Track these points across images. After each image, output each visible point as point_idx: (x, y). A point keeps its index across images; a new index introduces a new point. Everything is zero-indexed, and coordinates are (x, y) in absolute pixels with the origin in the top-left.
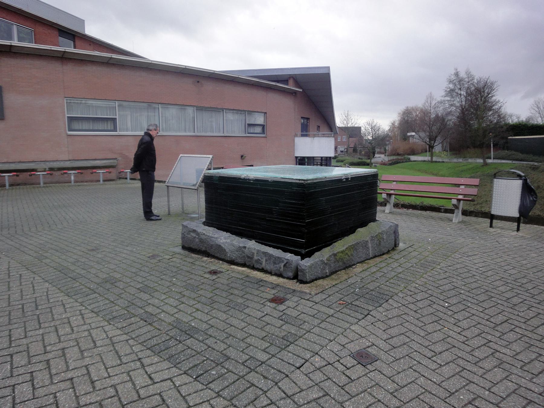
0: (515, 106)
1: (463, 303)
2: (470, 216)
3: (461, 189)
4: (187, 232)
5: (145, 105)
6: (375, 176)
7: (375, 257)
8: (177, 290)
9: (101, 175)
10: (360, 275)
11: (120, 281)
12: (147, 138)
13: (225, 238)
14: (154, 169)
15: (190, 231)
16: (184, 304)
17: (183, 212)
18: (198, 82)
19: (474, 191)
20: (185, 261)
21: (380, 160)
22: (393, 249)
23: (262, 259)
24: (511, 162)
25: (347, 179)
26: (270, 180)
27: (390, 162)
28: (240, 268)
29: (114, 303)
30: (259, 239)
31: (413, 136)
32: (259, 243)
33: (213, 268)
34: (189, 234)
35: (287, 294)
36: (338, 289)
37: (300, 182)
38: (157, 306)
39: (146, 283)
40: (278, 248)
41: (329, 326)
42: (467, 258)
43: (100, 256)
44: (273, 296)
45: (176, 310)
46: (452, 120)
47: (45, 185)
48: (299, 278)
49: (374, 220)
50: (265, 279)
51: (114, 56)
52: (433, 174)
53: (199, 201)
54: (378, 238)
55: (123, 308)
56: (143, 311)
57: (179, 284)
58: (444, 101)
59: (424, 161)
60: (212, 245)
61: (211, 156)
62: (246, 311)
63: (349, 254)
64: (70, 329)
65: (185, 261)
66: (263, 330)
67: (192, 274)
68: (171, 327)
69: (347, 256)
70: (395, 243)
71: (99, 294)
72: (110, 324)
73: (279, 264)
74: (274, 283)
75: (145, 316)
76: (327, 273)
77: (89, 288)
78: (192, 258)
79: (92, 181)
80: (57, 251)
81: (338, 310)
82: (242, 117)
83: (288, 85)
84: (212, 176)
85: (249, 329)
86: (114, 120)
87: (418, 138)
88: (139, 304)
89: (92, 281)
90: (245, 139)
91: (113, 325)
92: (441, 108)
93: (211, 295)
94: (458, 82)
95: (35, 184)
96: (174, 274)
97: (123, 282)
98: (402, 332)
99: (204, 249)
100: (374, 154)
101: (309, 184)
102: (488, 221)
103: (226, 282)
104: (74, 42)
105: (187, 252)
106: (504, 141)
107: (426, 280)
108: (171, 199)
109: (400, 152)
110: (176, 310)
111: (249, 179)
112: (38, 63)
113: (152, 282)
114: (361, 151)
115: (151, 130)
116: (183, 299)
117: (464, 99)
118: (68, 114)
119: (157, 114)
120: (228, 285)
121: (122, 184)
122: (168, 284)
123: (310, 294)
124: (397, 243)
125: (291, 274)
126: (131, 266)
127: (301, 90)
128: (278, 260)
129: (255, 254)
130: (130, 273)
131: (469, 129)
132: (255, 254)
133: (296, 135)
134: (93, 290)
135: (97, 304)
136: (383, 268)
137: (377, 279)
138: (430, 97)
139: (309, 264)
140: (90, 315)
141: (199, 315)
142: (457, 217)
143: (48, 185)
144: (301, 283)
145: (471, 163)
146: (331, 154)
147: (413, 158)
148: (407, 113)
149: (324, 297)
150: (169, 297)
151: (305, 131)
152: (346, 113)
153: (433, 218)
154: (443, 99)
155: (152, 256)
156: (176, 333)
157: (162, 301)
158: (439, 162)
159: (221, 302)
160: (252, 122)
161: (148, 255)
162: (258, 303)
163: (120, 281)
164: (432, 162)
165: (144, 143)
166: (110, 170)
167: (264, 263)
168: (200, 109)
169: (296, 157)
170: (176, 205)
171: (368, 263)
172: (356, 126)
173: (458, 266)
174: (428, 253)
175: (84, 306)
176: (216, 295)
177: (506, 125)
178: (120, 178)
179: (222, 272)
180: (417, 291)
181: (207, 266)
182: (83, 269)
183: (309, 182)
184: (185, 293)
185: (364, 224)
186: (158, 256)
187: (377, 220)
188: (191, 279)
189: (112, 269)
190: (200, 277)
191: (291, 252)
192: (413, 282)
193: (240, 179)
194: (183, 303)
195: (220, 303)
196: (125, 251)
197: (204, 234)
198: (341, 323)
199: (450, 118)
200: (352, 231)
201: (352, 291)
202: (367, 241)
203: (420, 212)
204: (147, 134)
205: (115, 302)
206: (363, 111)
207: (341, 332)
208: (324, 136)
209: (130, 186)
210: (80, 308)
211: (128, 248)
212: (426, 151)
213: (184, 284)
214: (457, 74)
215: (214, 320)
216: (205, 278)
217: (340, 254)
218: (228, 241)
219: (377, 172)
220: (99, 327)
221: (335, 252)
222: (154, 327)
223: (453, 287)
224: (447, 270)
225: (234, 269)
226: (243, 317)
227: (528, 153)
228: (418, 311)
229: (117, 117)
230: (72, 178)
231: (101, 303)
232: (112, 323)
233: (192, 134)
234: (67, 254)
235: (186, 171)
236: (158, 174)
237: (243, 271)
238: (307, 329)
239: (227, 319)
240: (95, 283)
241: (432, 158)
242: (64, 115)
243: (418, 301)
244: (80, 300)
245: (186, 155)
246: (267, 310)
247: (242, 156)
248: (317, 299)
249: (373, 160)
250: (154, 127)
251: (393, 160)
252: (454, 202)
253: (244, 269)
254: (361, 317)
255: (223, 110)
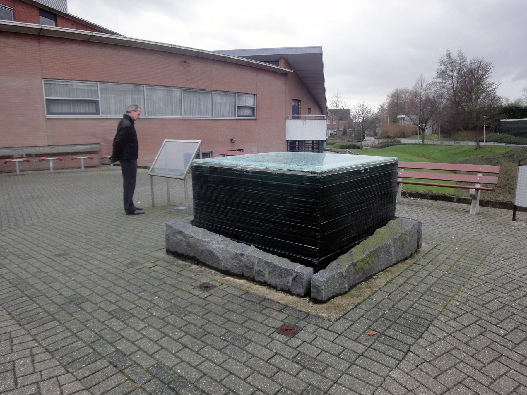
0: (510, 88)
1: (521, 328)
2: (486, 206)
3: (479, 177)
4: (172, 232)
5: (131, 87)
6: (394, 165)
7: (398, 262)
8: (158, 314)
9: (82, 161)
10: (386, 290)
11: (88, 300)
12: (127, 123)
13: (218, 243)
14: (136, 156)
15: (175, 233)
16: (167, 338)
17: (169, 204)
18: (185, 62)
19: (494, 180)
20: (169, 270)
21: (370, 143)
22: (416, 252)
23: (264, 270)
24: (504, 145)
25: (366, 170)
26: (273, 172)
27: (381, 145)
28: (237, 281)
29: (76, 336)
30: (260, 244)
31: (403, 119)
32: (260, 248)
33: (204, 280)
34: (174, 236)
35: (300, 320)
36: (363, 312)
37: (313, 175)
38: (133, 340)
39: (120, 304)
40: (284, 256)
41: (362, 373)
42: (503, 262)
43: (67, 263)
44: (282, 324)
45: (156, 348)
46: (444, 101)
47: (22, 173)
48: (312, 295)
49: (393, 217)
50: (269, 297)
51: (95, 34)
52: (425, 157)
53: (186, 191)
54: (401, 240)
55: (88, 345)
56: (114, 349)
57: (161, 304)
58: (436, 83)
59: (415, 144)
60: (202, 251)
61: (199, 141)
62: (249, 348)
63: (370, 262)
64: (13, 380)
65: (169, 270)
66: (273, 381)
67: (178, 289)
68: (149, 376)
69: (367, 265)
70: (418, 243)
71: (59, 322)
72: (68, 372)
73: (286, 277)
74: (281, 302)
75: (115, 357)
76: (345, 288)
77: (48, 312)
78: (178, 265)
79: (73, 168)
80: (18, 257)
81: (368, 344)
82: (231, 99)
83: (278, 65)
84: (202, 167)
85: (255, 380)
86: (96, 102)
87: (410, 120)
88: (108, 337)
89: (53, 302)
90: (235, 122)
91: (72, 373)
92: (432, 90)
93: (203, 322)
94: (450, 62)
95: (11, 171)
96: (156, 290)
97: (92, 302)
98: (459, 380)
99: (192, 254)
100: (364, 136)
101: (324, 178)
102: (511, 212)
103: (220, 301)
104: (56, 21)
105: (172, 258)
106: (497, 123)
107: (466, 295)
108: (155, 187)
109: (391, 135)
110: (156, 348)
111: (246, 171)
112: (13, 41)
113: (127, 303)
114: (350, 134)
115: (130, 112)
116: (166, 328)
117: (455, 80)
118: (46, 96)
119: (142, 97)
120: (223, 306)
121: (105, 170)
122: (148, 305)
123: (329, 320)
124: (420, 243)
125: (301, 291)
126: (104, 279)
127: (292, 71)
128: (287, 272)
129: (256, 264)
130: (102, 288)
131: (464, 112)
132: (256, 264)
133: (287, 118)
134: (51, 315)
135: (54, 338)
136: (410, 278)
137: (407, 294)
138: (421, 79)
139: (324, 279)
140: (43, 356)
141: (186, 354)
142: (474, 208)
143: (25, 172)
144: (314, 303)
145: (463, 146)
146: (323, 137)
147: (403, 141)
148: (396, 97)
149: (348, 325)
150: (149, 325)
151: (296, 114)
152: (336, 95)
153: (445, 208)
154: (434, 80)
155: (130, 263)
156: (156, 386)
157: (139, 331)
158: (430, 145)
159: (215, 333)
160: (241, 104)
161: (125, 263)
162: (263, 334)
163: (88, 300)
164: (423, 145)
165: (124, 128)
166: (93, 155)
167: (267, 275)
168: (187, 90)
169: (288, 141)
170: (160, 197)
171: (391, 271)
172: (345, 108)
173: (498, 273)
174: (457, 257)
175: (37, 341)
176: (209, 321)
177: (501, 107)
178: (104, 164)
179: (215, 287)
180: (460, 312)
181: (196, 278)
182: (45, 283)
183: (323, 175)
184: (168, 319)
185: (383, 223)
186: (137, 263)
187: (396, 217)
188: (177, 296)
189: (80, 283)
190: (187, 294)
191: (301, 262)
192: (452, 298)
193: (235, 170)
194: (166, 335)
195: (214, 335)
196: (99, 257)
197: (193, 237)
198: (377, 368)
199: (441, 100)
200: (370, 232)
201: (381, 314)
202: (390, 245)
203: (430, 201)
204: (127, 117)
205: (78, 334)
206: (352, 93)
207: (380, 382)
208: (315, 118)
209: (113, 173)
210: (31, 345)
211: (102, 252)
212: (417, 134)
213: (169, 304)
214: (449, 56)
215: (207, 363)
216: (194, 295)
217: (361, 263)
218: (222, 246)
219: (397, 160)
220: (53, 377)
221: (355, 261)
222: (127, 376)
223: (501, 305)
224: (487, 280)
225: (229, 281)
226: (245, 359)
227: (521, 135)
228: (470, 343)
229: (99, 99)
230: (51, 165)
231: (60, 335)
232: (70, 370)
233: (179, 117)
234: (29, 261)
235: (171, 158)
236: (140, 161)
237: (241, 284)
238: (333, 379)
239: (224, 362)
240: (56, 304)
241: (423, 141)
242: (43, 97)
243: (466, 327)
244: (33, 332)
245: (171, 140)
246: (277, 346)
247: (232, 140)
248: (340, 327)
249: (364, 143)
250: (134, 108)
251: (384, 143)
252: (472, 191)
253: (242, 281)
254: (400, 355)
255: (211, 91)
